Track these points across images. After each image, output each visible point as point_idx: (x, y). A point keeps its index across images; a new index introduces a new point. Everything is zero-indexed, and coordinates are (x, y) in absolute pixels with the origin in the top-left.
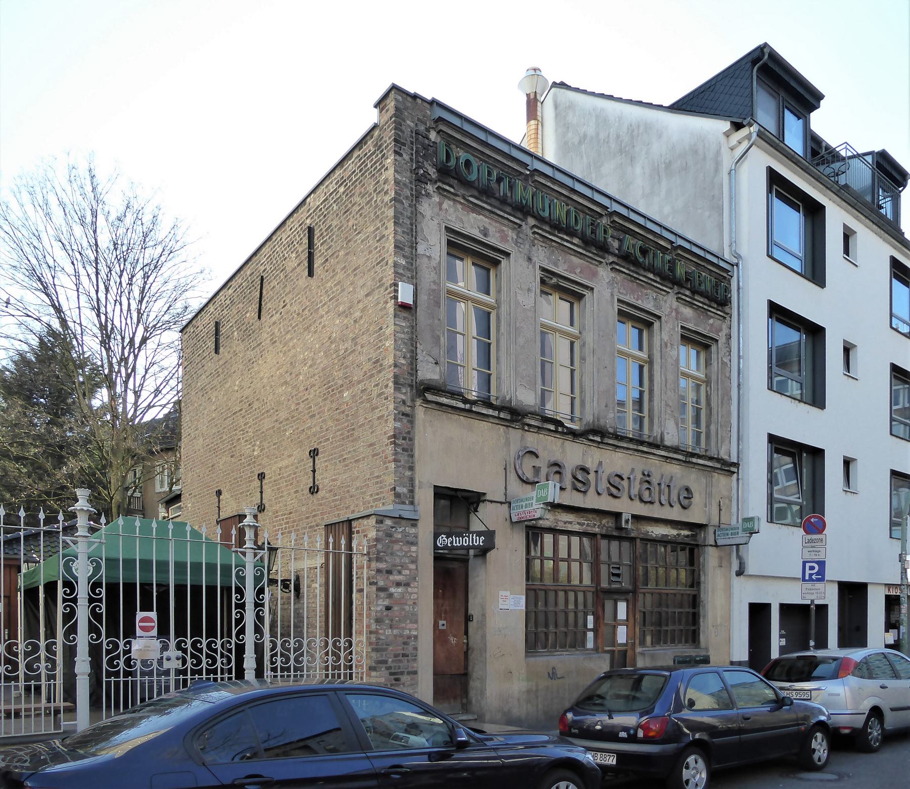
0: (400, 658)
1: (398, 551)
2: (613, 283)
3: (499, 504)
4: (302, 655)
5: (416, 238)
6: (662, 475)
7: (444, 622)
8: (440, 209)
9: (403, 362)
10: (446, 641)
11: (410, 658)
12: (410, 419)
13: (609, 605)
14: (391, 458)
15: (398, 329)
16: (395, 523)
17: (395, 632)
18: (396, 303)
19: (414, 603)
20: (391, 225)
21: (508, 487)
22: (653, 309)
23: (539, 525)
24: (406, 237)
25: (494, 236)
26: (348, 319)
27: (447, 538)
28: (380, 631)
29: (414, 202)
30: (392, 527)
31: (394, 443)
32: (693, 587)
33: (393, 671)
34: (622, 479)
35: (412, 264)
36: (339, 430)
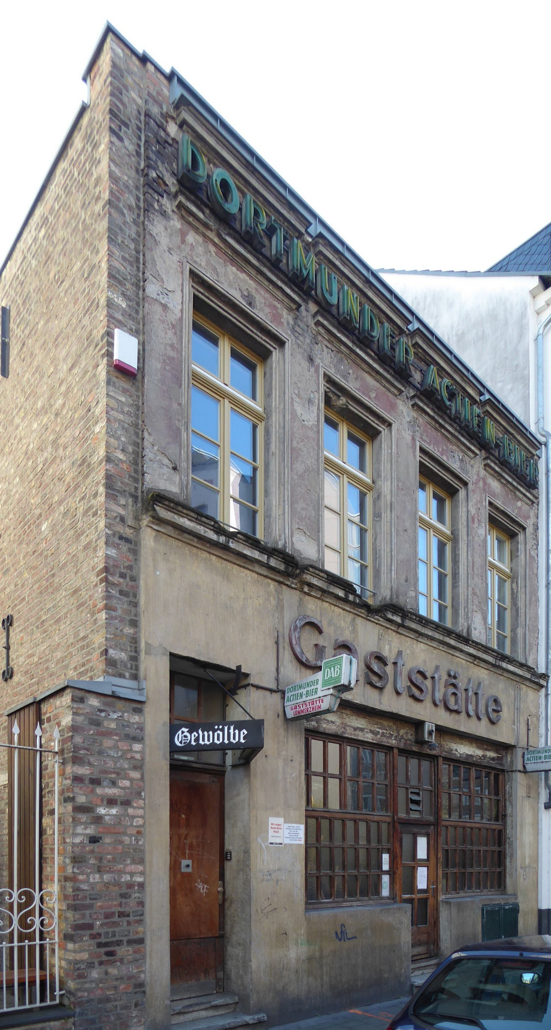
0: (116, 919)
1: (110, 748)
2: (413, 425)
3: (268, 693)
4: (21, 907)
5: (144, 273)
6: (469, 680)
7: (189, 862)
8: (183, 241)
9: (121, 456)
10: (193, 890)
11: (131, 918)
12: (132, 547)
13: (406, 839)
14: (101, 605)
15: (113, 403)
16: (105, 704)
17: (106, 877)
18: (109, 364)
19: (139, 833)
20: (104, 246)
21: (282, 669)
22: (459, 470)
23: (321, 730)
24: (129, 268)
25: (261, 310)
26: (48, 416)
27: (190, 732)
28: (81, 877)
29: (142, 218)
30: (101, 711)
31: (106, 580)
32: (498, 821)
33: (103, 940)
34: (425, 677)
35: (137, 312)
36: (35, 583)
